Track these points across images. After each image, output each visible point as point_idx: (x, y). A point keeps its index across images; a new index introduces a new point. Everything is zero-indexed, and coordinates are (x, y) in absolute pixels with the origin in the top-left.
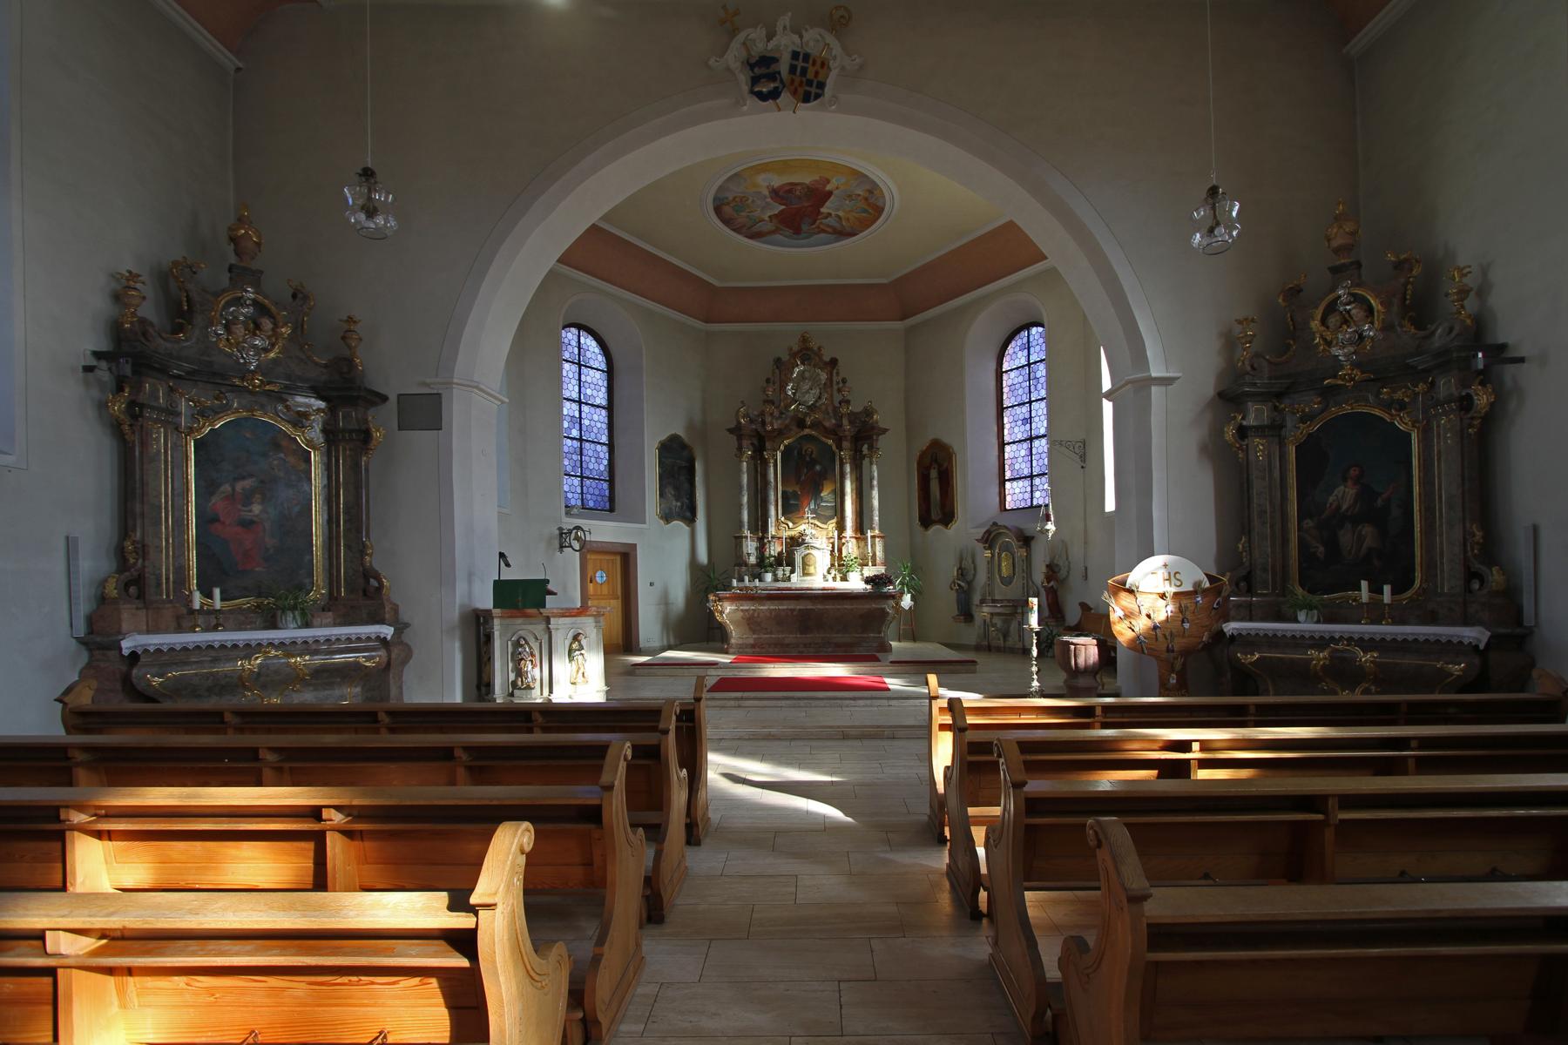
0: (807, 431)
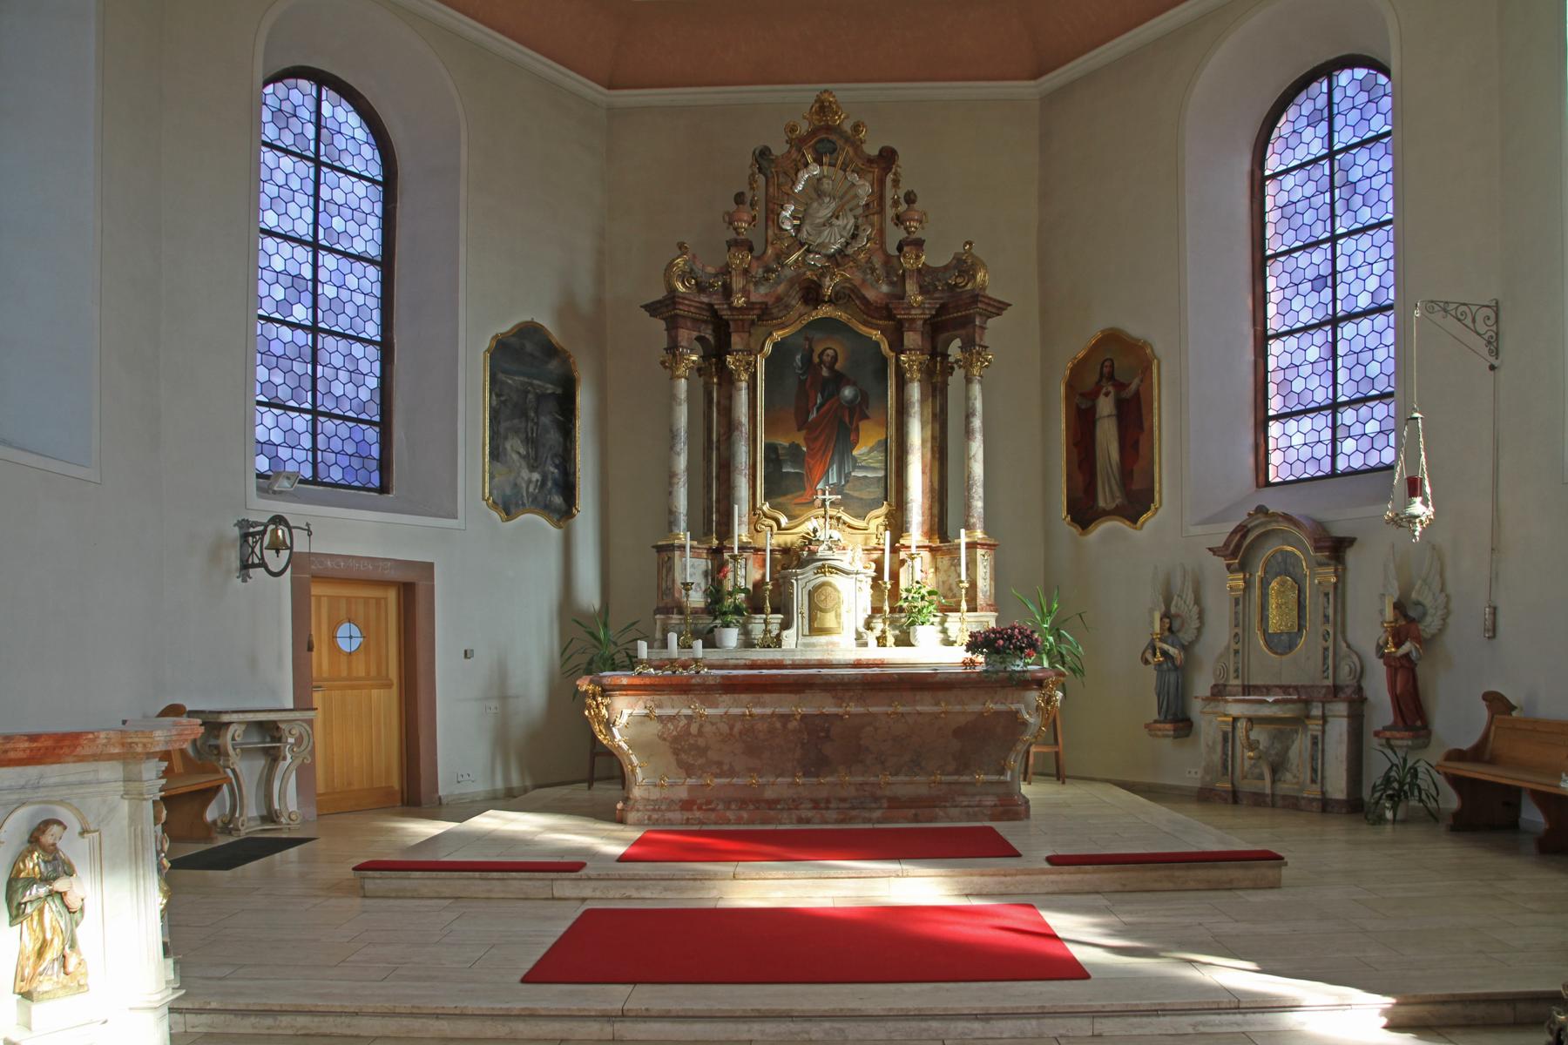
0: (824, 311)
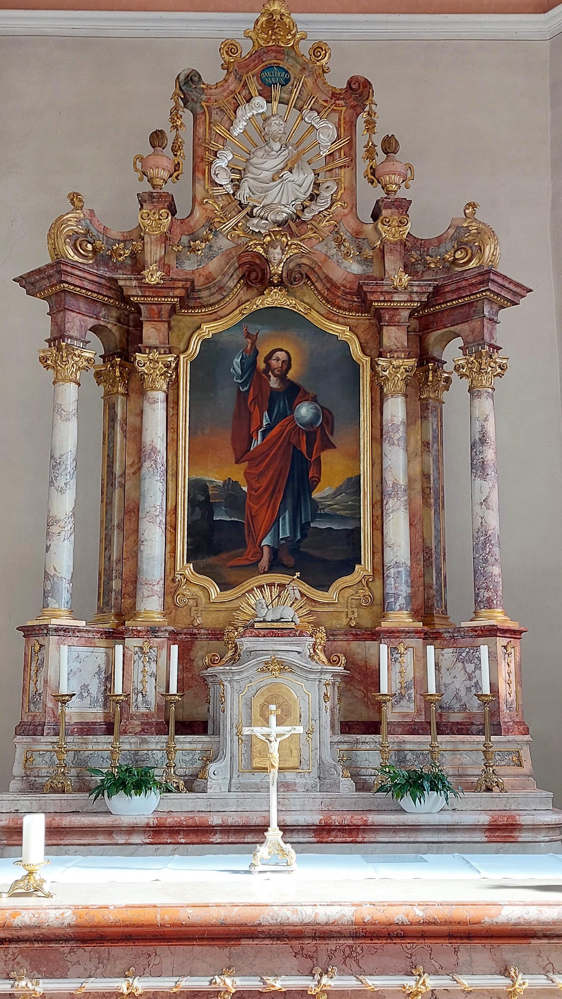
0: (274, 298)
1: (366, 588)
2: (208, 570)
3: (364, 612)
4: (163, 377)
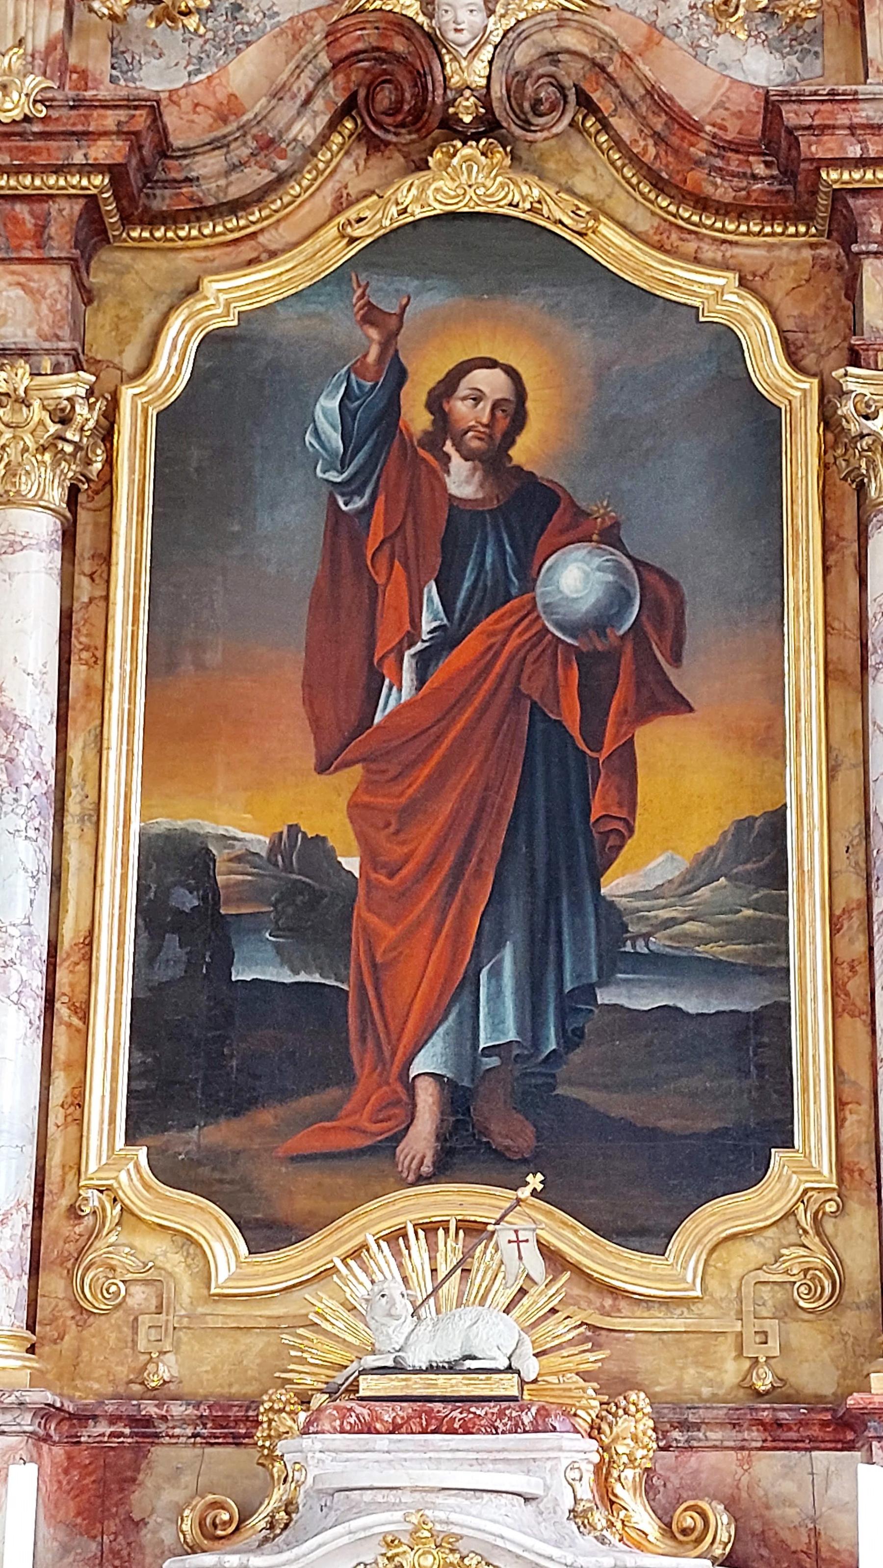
0: (464, 181)
1: (813, 1241)
2: (205, 1171)
3: (806, 1336)
4: (47, 457)
